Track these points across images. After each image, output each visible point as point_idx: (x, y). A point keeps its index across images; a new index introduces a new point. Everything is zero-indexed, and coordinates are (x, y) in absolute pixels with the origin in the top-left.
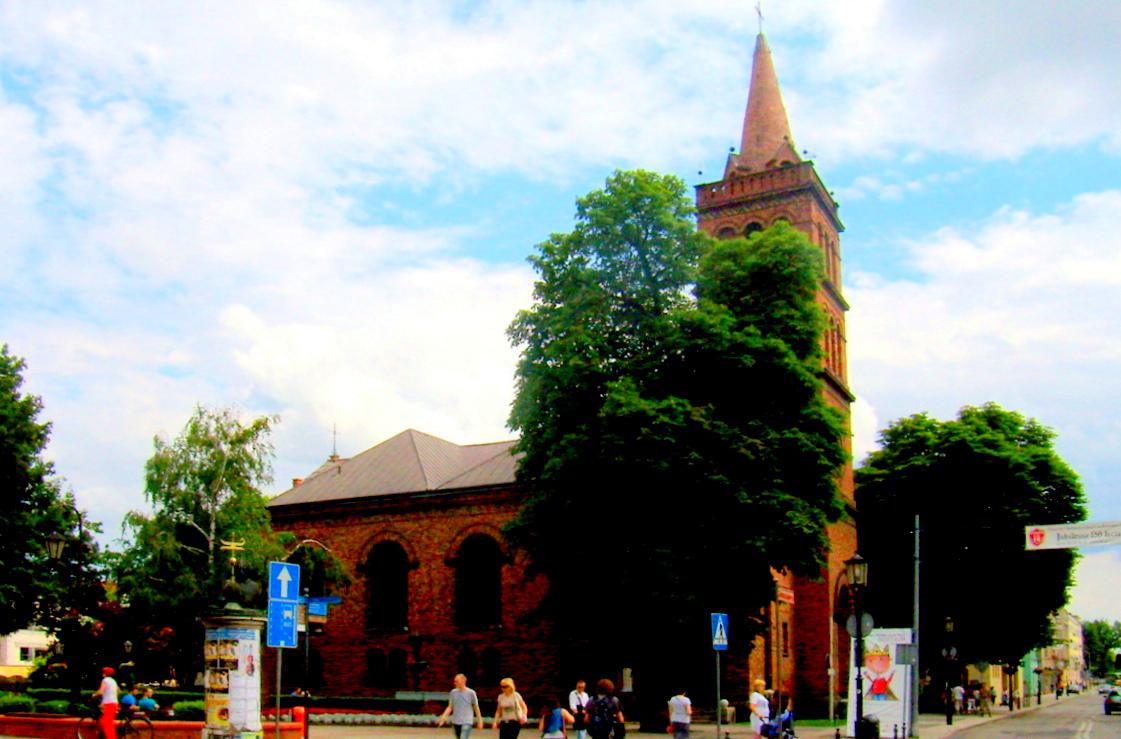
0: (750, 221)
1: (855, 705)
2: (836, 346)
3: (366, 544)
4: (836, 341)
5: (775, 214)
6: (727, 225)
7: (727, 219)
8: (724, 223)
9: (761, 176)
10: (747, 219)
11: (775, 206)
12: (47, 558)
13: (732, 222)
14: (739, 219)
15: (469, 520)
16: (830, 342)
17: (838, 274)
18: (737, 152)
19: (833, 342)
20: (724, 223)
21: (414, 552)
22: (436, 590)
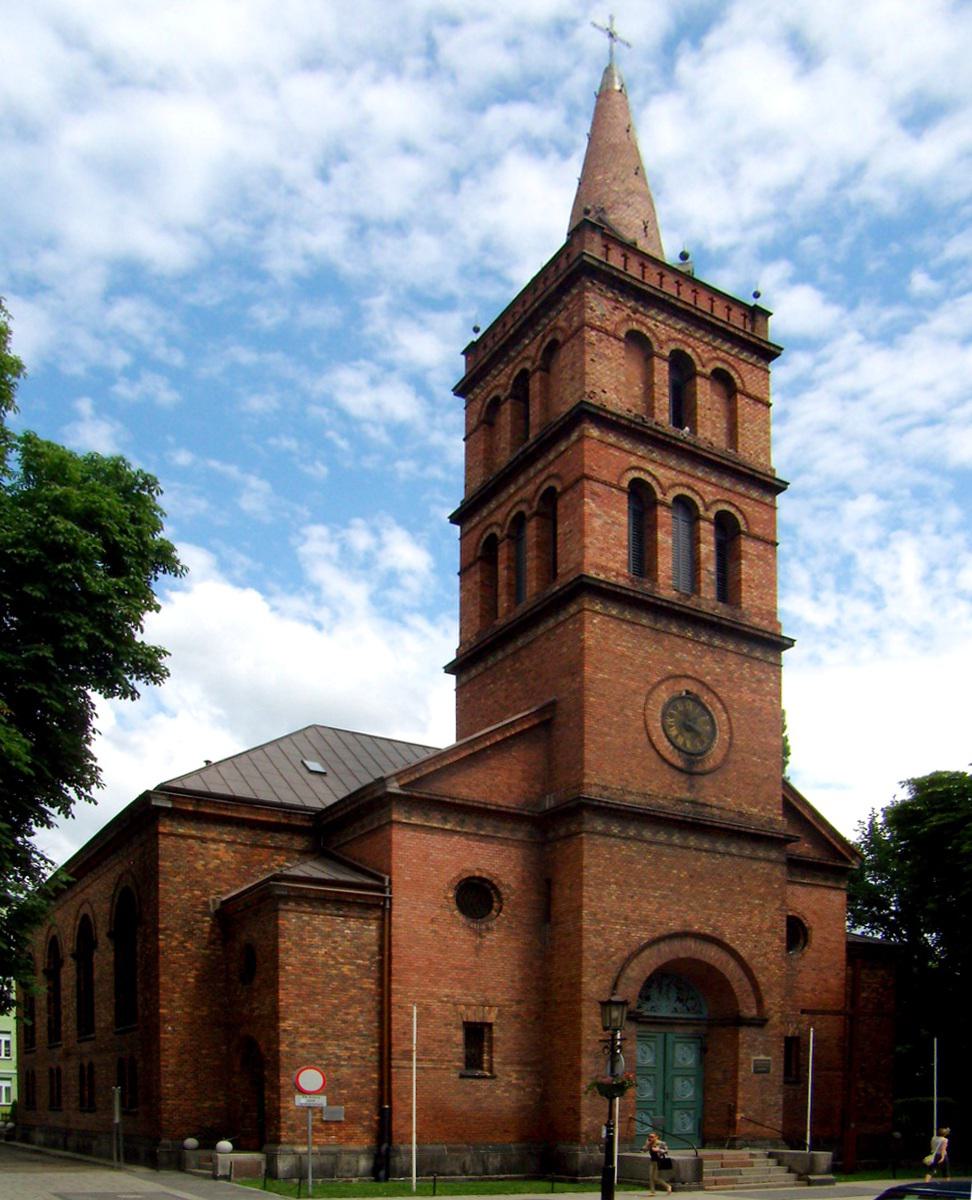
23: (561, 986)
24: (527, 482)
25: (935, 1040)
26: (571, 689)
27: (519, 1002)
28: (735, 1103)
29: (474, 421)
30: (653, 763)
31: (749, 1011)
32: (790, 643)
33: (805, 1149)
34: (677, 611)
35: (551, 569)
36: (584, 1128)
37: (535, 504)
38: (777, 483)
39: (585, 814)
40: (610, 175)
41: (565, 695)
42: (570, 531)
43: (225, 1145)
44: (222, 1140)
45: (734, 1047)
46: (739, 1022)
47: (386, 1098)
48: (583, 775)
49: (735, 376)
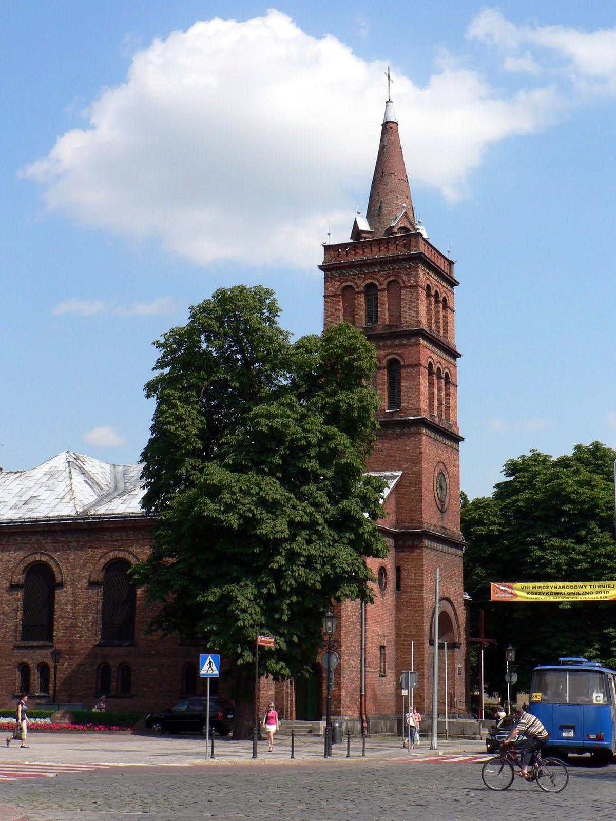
2: (443, 393)
4: (443, 387)
16: (435, 391)
19: (440, 389)
20: (346, 281)
22: (80, 608)
30: (436, 509)
32: (462, 439)
42: (411, 388)
48: (422, 517)
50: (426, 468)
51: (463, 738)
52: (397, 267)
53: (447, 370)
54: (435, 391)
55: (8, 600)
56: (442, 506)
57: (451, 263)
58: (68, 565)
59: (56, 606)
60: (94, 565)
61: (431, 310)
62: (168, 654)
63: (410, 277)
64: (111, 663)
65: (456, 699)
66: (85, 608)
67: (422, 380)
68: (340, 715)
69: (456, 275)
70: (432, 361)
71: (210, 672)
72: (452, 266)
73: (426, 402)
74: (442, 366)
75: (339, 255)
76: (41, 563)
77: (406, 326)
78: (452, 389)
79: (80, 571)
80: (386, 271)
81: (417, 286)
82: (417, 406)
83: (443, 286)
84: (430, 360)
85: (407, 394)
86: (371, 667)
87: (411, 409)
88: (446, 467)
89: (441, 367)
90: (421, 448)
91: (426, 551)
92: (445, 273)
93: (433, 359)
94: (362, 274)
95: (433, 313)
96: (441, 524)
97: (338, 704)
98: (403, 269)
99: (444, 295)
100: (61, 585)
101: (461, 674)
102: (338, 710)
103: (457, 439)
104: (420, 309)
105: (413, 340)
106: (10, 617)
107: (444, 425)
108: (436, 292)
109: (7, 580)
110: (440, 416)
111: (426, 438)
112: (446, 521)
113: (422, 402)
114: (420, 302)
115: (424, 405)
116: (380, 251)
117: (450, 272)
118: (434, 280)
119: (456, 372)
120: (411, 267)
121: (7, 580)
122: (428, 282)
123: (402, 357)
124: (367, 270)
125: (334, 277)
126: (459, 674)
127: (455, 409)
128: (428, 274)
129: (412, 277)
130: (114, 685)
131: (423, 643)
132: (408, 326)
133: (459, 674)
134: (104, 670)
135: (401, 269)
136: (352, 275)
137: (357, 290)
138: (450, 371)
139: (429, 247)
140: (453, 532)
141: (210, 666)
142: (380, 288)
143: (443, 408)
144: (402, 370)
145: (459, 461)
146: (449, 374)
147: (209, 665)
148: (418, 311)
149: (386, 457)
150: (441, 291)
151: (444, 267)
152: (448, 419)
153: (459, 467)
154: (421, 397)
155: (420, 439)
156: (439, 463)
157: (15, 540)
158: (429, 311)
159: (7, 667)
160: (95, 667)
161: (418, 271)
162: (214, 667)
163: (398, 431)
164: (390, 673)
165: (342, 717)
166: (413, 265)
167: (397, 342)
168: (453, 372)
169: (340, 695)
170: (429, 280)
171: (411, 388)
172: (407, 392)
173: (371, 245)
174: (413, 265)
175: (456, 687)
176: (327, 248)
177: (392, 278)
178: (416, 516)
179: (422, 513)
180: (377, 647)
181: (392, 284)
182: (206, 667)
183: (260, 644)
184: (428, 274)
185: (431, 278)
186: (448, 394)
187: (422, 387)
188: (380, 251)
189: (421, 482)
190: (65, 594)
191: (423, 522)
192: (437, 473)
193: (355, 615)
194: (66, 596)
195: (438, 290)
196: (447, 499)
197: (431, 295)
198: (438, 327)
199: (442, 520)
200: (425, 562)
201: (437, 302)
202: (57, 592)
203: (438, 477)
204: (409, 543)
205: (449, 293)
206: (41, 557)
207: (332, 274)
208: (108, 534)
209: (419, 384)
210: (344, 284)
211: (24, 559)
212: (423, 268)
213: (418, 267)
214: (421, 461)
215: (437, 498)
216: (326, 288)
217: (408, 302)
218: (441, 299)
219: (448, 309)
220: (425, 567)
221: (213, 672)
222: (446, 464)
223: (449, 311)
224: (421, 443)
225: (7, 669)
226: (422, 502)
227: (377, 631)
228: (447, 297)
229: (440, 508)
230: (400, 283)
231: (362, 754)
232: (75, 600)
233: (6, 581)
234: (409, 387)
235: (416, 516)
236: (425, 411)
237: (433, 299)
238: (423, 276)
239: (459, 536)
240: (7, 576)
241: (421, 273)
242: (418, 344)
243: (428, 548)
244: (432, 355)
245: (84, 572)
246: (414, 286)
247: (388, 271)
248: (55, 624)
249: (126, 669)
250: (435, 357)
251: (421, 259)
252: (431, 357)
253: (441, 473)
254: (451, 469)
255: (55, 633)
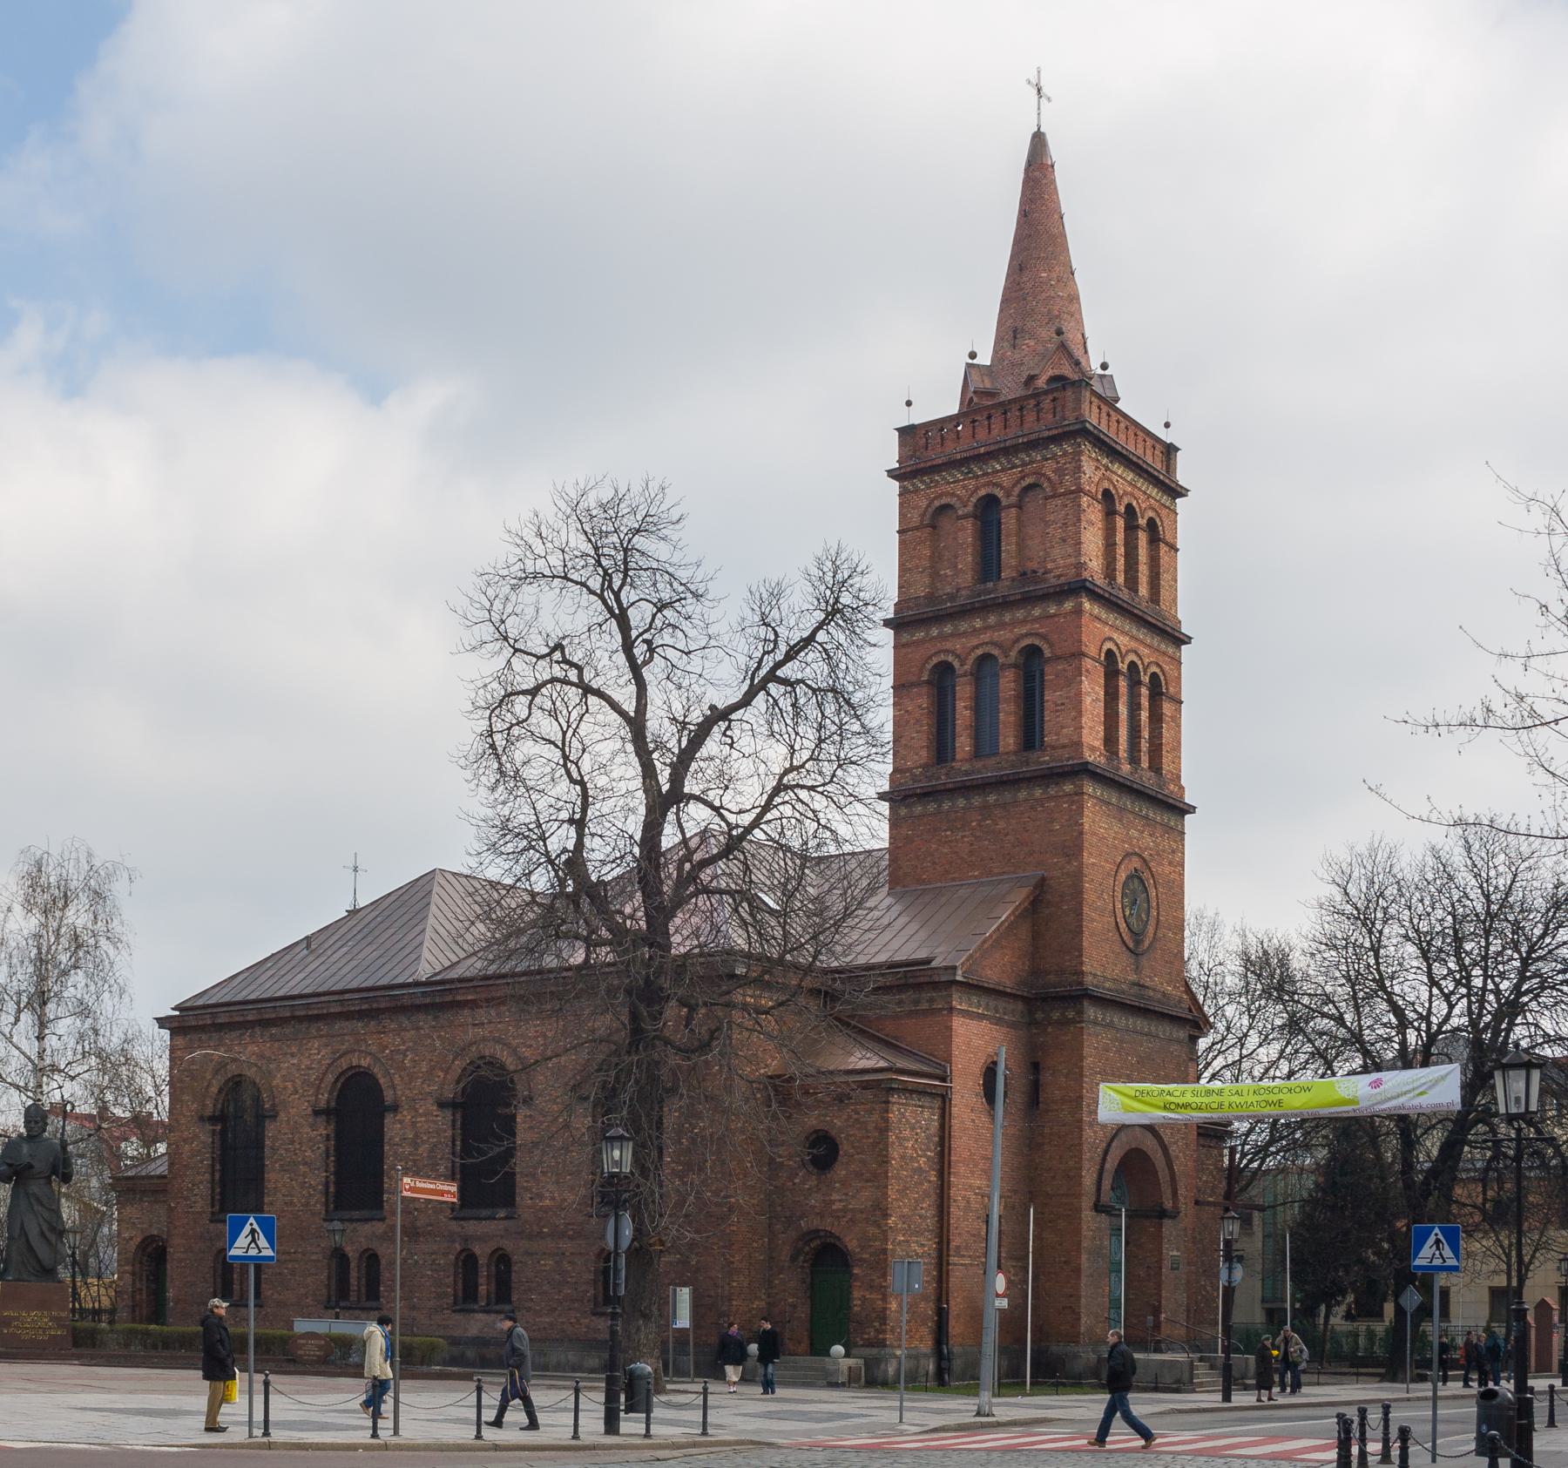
0: (982, 492)
1: (1311, 1409)
2: (1144, 715)
3: (324, 1074)
4: (1145, 702)
5: (1023, 478)
6: (944, 501)
7: (949, 488)
8: (940, 496)
9: (1020, 403)
10: (977, 488)
11: (1024, 464)
12: (1391, 1016)
13: (953, 495)
14: (964, 487)
15: (471, 1033)
16: (1123, 710)
17: (1165, 578)
18: (985, 359)
19: (1134, 708)
20: (940, 496)
21: (393, 1087)
22: (423, 1149)
23: (1054, 1178)
24: (1001, 625)
25: (1032, 1210)
26: (1065, 871)
27: (1015, 1192)
28: (1160, 1302)
29: (915, 519)
30: (1118, 947)
31: (1168, 1204)
32: (1191, 809)
33: (533, 1370)
34: (1171, 804)
35: (1031, 735)
36: (1083, 1329)
37: (1013, 654)
38: (1181, 636)
39: (1086, 1003)
40: (1054, 275)
41: (1057, 873)
42: (1063, 704)
43: (838, 1349)
44: (836, 1344)
45: (1158, 1237)
46: (1162, 1214)
47: (944, 1299)
48: (1082, 963)
49: (1159, 524)
50: (1093, 864)
51: (1156, 1390)
52: (1039, 458)
53: (1154, 669)
54: (1123, 710)
55: (310, 1140)
56: (1138, 942)
57: (1170, 451)
58: (402, 1073)
59: (386, 1148)
60: (446, 1071)
61: (1116, 544)
62: (571, 1233)
63: (1065, 475)
64: (477, 1250)
65: (1163, 1316)
66: (432, 1150)
67: (1086, 685)
68: (885, 1346)
69: (1182, 477)
70: (1114, 649)
71: (253, 1252)
72: (1172, 457)
73: (1098, 732)
74: (1141, 659)
75: (927, 443)
76: (362, 1070)
77: (1054, 577)
78: (1167, 708)
79: (422, 1083)
80: (1017, 467)
81: (1080, 490)
82: (1075, 738)
83: (1149, 496)
84: (1108, 645)
85: (1058, 716)
86: (964, 1256)
87: (1064, 747)
88: (1147, 865)
89: (1139, 663)
90: (1082, 824)
91: (1090, 1029)
92: (1155, 469)
93: (1117, 645)
94: (970, 478)
95: (1121, 550)
96: (1133, 977)
97: (881, 1324)
98: (1049, 459)
99: (1151, 514)
100: (395, 1108)
101: (1177, 1269)
102: (881, 1336)
103: (1183, 810)
104: (1083, 540)
105: (1068, 605)
106: (315, 1169)
107: (1147, 779)
108: (1129, 507)
109: (308, 1101)
110: (1134, 760)
111: (1094, 805)
112: (1147, 972)
113: (1085, 731)
114: (1083, 524)
115: (1092, 736)
116: (1005, 428)
117: (1168, 472)
118: (1122, 480)
119: (1180, 674)
120: (1065, 454)
121: (308, 1101)
122: (1106, 485)
123: (1048, 641)
124: (981, 469)
125: (917, 490)
126: (1172, 1269)
127: (1177, 748)
128: (1107, 469)
129: (1067, 475)
130: (483, 1289)
131: (1079, 1210)
132: (1059, 576)
133: (1172, 1269)
134: (468, 1262)
135: (1047, 459)
136: (952, 483)
137: (960, 512)
138: (1162, 670)
139: (1112, 413)
140: (1164, 994)
141: (254, 1240)
142: (1004, 503)
143: (1144, 746)
144: (1047, 669)
145: (1183, 853)
146: (1162, 678)
147: (250, 1238)
148: (1080, 543)
149: (1014, 846)
150: (1143, 506)
151: (1154, 461)
152: (1156, 767)
153: (1183, 866)
154: (1084, 720)
155: (1081, 807)
156: (1128, 855)
157: (319, 1029)
158: (1110, 546)
159: (314, 1257)
160: (452, 1257)
161: (1080, 460)
162: (263, 1242)
163: (1038, 792)
164: (1013, 1266)
165: (888, 1350)
166: (1070, 450)
167: (1037, 612)
168: (1171, 673)
169: (885, 1309)
170: (1110, 480)
171: (1063, 704)
172: (1057, 711)
173: (989, 417)
174: (1070, 450)
175: (1164, 1294)
176: (906, 433)
177: (1028, 481)
178: (1070, 961)
179: (1081, 956)
180: (978, 1218)
181: (1031, 493)
182: (242, 1241)
183: (405, 1194)
184: (1107, 469)
185: (1115, 478)
186: (1156, 718)
187: (1088, 700)
188: (1005, 428)
189: (1081, 892)
190: (399, 1126)
191: (1082, 973)
192: (1123, 876)
193: (925, 1156)
194: (400, 1129)
195: (1134, 503)
196: (1151, 929)
197: (1138, 527)
198: (1132, 583)
199: (1137, 970)
200: (1086, 1051)
201: (1131, 528)
202: (389, 1119)
203: (1125, 884)
204: (1056, 1015)
205: (1164, 512)
206: (359, 1059)
207: (913, 485)
208: (466, 1012)
209: (1079, 694)
210: (937, 503)
211: (332, 1063)
212: (1094, 455)
213: (1081, 453)
214: (1080, 849)
215: (1123, 926)
216: (902, 515)
217: (1060, 528)
218: (1142, 522)
219: (1162, 545)
220: (1088, 1061)
221: (260, 1252)
222: (1148, 858)
223: (1163, 548)
224: (1081, 814)
225: (315, 1261)
226: (1082, 932)
227: (979, 1188)
228: (1158, 520)
229: (1131, 945)
230: (1044, 489)
231: (644, 1432)
232: (417, 1136)
233: (306, 1104)
234: (1059, 702)
235: (1070, 961)
236: (1093, 749)
237: (1120, 523)
238: (1092, 470)
239: (1180, 1002)
240: (308, 1096)
241: (1088, 467)
242: (1078, 611)
243: (1095, 1023)
244: (1115, 636)
245: (429, 1086)
246: (1072, 492)
247: (1021, 466)
248: (386, 1180)
249: (502, 1260)
250: (1144, 651)
251: (1083, 433)
252: (1110, 639)
253: (1135, 876)
254: (1162, 869)
255: (385, 1197)
